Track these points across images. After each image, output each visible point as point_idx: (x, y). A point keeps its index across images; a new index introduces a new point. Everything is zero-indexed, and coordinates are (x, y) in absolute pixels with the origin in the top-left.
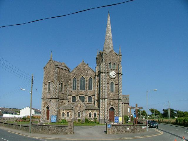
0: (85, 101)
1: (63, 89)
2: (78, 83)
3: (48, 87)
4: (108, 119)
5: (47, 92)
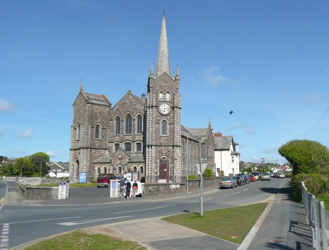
0: (132, 149)
1: (100, 134)
2: (124, 124)
3: (78, 132)
4: (158, 175)
5: (77, 139)
